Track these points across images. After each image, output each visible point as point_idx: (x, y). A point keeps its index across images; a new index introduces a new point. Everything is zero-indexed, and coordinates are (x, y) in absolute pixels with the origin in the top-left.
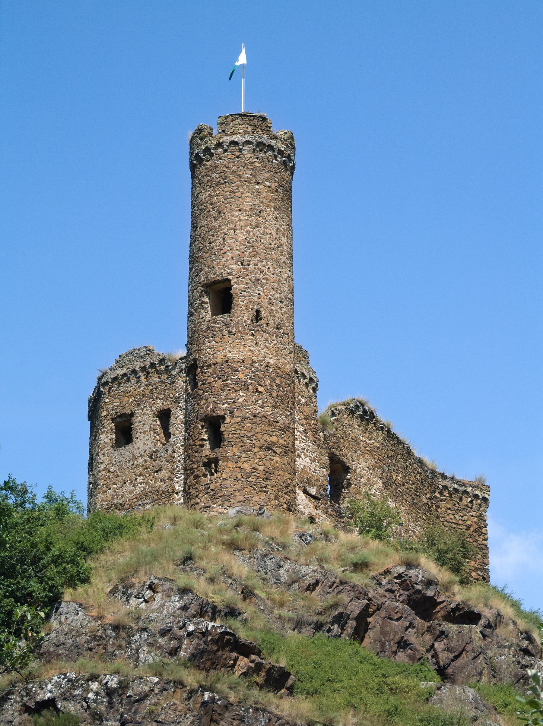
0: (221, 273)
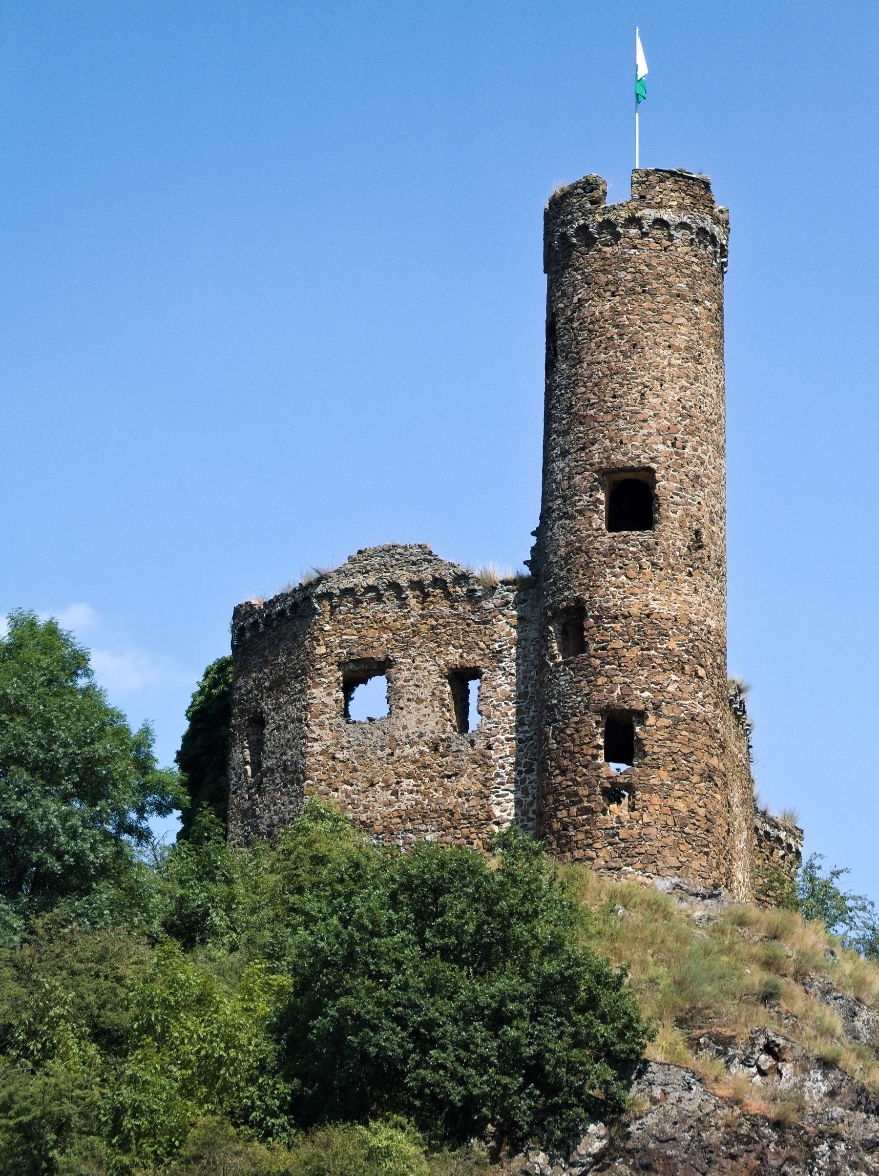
0: (638, 456)
